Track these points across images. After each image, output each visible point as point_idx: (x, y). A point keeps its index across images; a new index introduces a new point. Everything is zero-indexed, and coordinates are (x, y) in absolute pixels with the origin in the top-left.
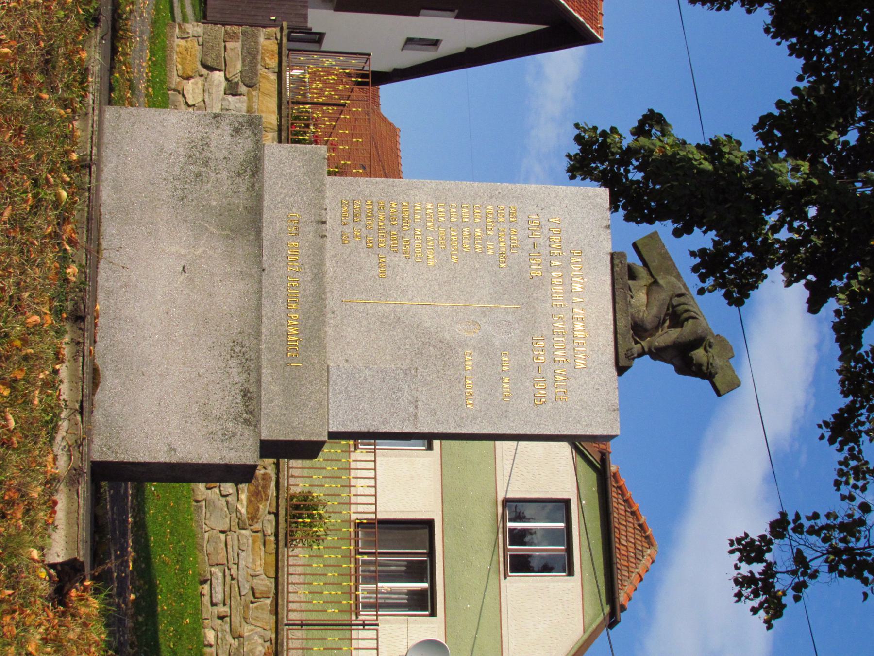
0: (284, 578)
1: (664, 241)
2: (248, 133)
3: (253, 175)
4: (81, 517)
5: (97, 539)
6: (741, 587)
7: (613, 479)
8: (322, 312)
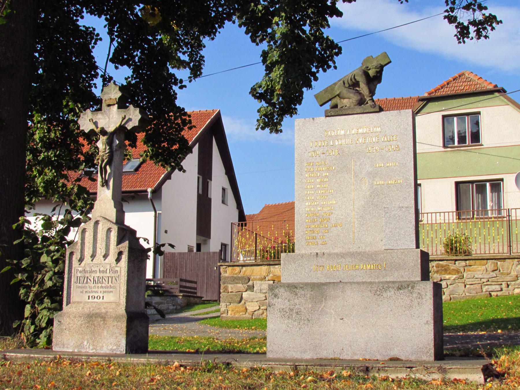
0: (487, 256)
1: (319, 92)
2: (277, 290)
3: (296, 288)
4: (462, 367)
5: (471, 355)
6: (482, 36)
7: (431, 95)
8: (359, 254)
